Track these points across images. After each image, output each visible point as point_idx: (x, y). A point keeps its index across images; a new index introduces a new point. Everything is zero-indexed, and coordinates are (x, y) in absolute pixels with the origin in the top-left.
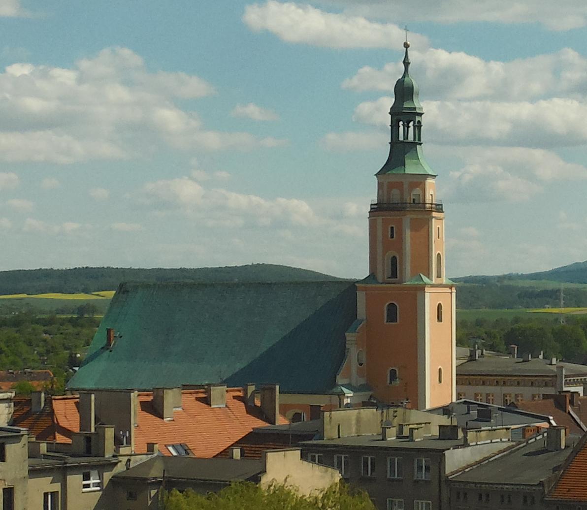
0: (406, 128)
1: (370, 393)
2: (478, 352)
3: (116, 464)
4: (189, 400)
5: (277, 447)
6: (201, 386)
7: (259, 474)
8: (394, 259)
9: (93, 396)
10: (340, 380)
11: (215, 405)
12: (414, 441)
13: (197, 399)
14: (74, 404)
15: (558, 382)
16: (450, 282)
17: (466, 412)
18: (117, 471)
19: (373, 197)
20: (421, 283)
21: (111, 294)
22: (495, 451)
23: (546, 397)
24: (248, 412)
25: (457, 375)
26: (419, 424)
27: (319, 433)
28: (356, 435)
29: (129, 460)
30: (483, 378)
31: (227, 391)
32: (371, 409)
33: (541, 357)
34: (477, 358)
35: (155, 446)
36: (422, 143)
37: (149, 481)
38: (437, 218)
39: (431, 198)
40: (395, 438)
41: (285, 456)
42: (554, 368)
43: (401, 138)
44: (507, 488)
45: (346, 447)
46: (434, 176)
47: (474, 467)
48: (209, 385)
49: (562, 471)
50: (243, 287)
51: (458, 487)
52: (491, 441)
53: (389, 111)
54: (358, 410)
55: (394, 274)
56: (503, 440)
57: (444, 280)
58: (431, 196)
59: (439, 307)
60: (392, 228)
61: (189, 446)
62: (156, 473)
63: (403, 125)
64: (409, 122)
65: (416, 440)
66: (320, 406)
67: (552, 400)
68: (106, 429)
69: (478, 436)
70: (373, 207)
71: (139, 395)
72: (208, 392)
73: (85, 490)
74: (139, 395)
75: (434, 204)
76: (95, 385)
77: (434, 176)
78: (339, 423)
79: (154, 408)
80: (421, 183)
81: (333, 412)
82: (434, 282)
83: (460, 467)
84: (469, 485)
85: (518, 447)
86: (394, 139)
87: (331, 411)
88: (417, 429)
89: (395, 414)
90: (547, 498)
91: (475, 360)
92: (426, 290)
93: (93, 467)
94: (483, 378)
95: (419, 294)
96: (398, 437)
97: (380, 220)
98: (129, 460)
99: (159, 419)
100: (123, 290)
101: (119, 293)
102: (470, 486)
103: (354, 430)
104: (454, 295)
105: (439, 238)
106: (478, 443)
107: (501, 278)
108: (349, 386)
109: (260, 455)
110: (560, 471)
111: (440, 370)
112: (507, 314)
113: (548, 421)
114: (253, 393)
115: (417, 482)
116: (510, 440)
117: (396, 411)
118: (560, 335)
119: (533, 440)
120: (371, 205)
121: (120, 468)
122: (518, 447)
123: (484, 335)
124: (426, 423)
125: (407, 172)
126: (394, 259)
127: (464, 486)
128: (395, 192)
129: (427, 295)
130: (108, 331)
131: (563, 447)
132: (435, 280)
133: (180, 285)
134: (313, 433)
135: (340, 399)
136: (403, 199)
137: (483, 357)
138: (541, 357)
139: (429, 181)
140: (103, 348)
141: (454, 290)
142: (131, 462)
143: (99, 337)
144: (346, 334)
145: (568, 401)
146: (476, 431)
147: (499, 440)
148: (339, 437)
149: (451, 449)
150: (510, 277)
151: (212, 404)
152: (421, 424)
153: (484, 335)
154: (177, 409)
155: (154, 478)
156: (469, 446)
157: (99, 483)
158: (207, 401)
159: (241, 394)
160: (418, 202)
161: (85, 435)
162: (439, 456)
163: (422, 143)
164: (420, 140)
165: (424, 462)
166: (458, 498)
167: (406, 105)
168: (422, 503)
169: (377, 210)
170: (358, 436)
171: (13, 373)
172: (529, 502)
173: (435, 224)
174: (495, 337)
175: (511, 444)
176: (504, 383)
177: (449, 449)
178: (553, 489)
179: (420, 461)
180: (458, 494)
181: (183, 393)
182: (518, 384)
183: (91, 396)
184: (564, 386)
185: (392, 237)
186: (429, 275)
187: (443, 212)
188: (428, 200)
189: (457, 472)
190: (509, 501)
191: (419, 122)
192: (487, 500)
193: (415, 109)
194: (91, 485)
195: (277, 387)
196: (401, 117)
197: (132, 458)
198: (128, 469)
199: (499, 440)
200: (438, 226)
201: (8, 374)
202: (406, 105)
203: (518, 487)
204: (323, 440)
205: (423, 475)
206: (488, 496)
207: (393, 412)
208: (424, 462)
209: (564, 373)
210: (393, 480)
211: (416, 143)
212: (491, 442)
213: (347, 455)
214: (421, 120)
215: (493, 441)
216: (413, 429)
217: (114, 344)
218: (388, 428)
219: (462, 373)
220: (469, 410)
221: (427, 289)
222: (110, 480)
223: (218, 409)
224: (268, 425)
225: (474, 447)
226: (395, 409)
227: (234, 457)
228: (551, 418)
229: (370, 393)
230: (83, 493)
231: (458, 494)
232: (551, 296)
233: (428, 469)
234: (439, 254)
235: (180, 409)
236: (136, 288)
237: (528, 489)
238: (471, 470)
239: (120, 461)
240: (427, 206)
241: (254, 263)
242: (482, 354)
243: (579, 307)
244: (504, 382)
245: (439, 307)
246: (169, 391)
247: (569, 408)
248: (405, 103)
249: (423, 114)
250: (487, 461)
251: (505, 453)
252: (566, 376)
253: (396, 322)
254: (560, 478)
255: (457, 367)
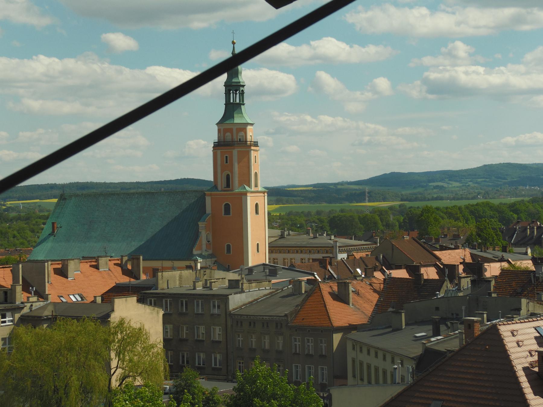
0: (235, 95)
1: (215, 259)
2: (286, 233)
3: (23, 308)
4: (86, 266)
5: (126, 294)
6: (94, 258)
7: (110, 312)
8: (228, 177)
9: (21, 266)
10: (195, 252)
11: (102, 269)
12: (213, 290)
13: (91, 266)
14: (10, 271)
15: (334, 251)
16: (264, 190)
17: (263, 270)
18: (24, 312)
19: (215, 137)
20: (245, 190)
21: (55, 200)
22: (262, 295)
23: (314, 260)
24: (123, 274)
25: (269, 247)
26: (218, 279)
27: (155, 286)
28: (180, 286)
29: (32, 305)
30: (288, 249)
31: (110, 260)
32: (189, 271)
33: (325, 235)
34: (285, 236)
35: (49, 296)
36: (245, 104)
37: (43, 318)
38: (254, 150)
39: (250, 138)
40: (202, 288)
41: (126, 300)
42: (331, 242)
43: (232, 101)
44: (266, 318)
45: (170, 294)
46: (252, 124)
47: (247, 305)
48: (98, 257)
49: (300, 307)
50: (137, 195)
51: (237, 318)
52: (259, 289)
53: (224, 84)
54: (180, 271)
55: (228, 185)
56: (267, 288)
57: (260, 189)
58: (250, 137)
59: (257, 205)
60: (227, 157)
61: (83, 295)
62: (47, 313)
63: (233, 93)
64: (236, 91)
65: (214, 289)
66: (158, 269)
67: (317, 263)
68: (17, 286)
69: (250, 286)
70: (215, 144)
71: (52, 264)
72: (97, 261)
73: (2, 324)
74: (52, 264)
75: (253, 142)
76: (44, 257)
77: (252, 124)
78: (168, 279)
79: (62, 272)
80: (245, 128)
81: (163, 273)
82: (253, 190)
83: (239, 305)
84: (243, 316)
85: (276, 292)
86: (227, 101)
87: (162, 272)
88: (214, 282)
89: (205, 273)
90: (290, 324)
91: (284, 237)
92: (248, 195)
93: (8, 310)
94: (288, 249)
95: (243, 197)
96: (204, 287)
97: (219, 152)
98: (32, 305)
99: (65, 279)
100: (62, 198)
101: (60, 200)
102: (244, 317)
103: (178, 283)
104: (266, 197)
105: (256, 162)
106: (250, 290)
107: (335, 184)
108: (201, 256)
109: (110, 300)
110: (299, 307)
111: (258, 244)
112: (337, 207)
113: (314, 275)
114: (126, 262)
115: (212, 315)
116: (271, 288)
117: (205, 271)
118: (364, 220)
119: (286, 288)
120: (214, 143)
121: (26, 310)
122: (276, 292)
123: (317, 221)
124: (222, 279)
125: (235, 122)
126: (228, 177)
127: (241, 317)
128: (228, 134)
129: (249, 198)
130: (52, 224)
131: (303, 292)
132: (253, 189)
133: (98, 194)
134: (152, 286)
135: (195, 263)
136: (233, 139)
137: (290, 236)
138: (325, 235)
139: (249, 127)
140: (49, 234)
141: (266, 194)
142: (33, 306)
143: (47, 229)
144: (199, 223)
145: (328, 263)
146: (249, 283)
147: (264, 288)
148: (168, 288)
149: (233, 294)
150: (342, 184)
151: (100, 268)
152: (219, 279)
153: (317, 221)
154: (77, 272)
155: (46, 316)
156: (244, 292)
157: (12, 320)
158: (97, 267)
159: (119, 262)
160: (242, 141)
161: (4, 290)
162: (224, 299)
163: (245, 104)
164: (243, 101)
165: (216, 302)
166: (237, 325)
167: (234, 80)
168: (202, 327)
169: (217, 146)
170: (181, 287)
171: (9, 251)
172: (279, 327)
173: (253, 154)
174: (323, 222)
175: (272, 290)
176: (310, 252)
177: (232, 294)
178: (294, 318)
179: (214, 302)
180: (237, 322)
181: (81, 262)
182: (310, 252)
183: (19, 265)
184: (338, 253)
185: (227, 162)
186: (249, 186)
187: (258, 146)
188: (249, 138)
189: (236, 309)
190: (268, 326)
191: (242, 90)
192: (254, 326)
193: (240, 82)
194: (7, 322)
195: (141, 257)
196: (231, 88)
197: (34, 304)
198: (31, 311)
199: (264, 288)
200: (255, 155)
201: (6, 252)
202: (234, 80)
203: (272, 317)
204: (158, 290)
205: (216, 311)
206: (255, 323)
207: (203, 272)
208: (216, 302)
209: (338, 245)
210: (198, 314)
211: (241, 104)
212: (259, 290)
213: (203, 300)
214: (243, 89)
215: (260, 289)
216: (211, 282)
217: (56, 232)
218: (197, 282)
219: (273, 246)
220: (264, 269)
221: (248, 194)
222: (19, 318)
223: (104, 271)
224: (132, 280)
225: (248, 293)
226: (205, 270)
227: (97, 302)
228: (315, 273)
229: (215, 259)
230: (1, 326)
231: (237, 322)
232: (359, 196)
233: (219, 307)
234: (256, 172)
235: (79, 272)
236: (71, 197)
237: (278, 319)
238: (246, 307)
239: (26, 306)
240: (248, 143)
241: (182, 178)
242: (289, 234)
243: (384, 202)
244: (327, 251)
245: (257, 205)
246: (72, 261)
247: (329, 267)
248: (233, 79)
249: (245, 85)
250: (256, 302)
251: (268, 296)
252: (339, 247)
253: (230, 215)
254: (298, 312)
255: (269, 244)
